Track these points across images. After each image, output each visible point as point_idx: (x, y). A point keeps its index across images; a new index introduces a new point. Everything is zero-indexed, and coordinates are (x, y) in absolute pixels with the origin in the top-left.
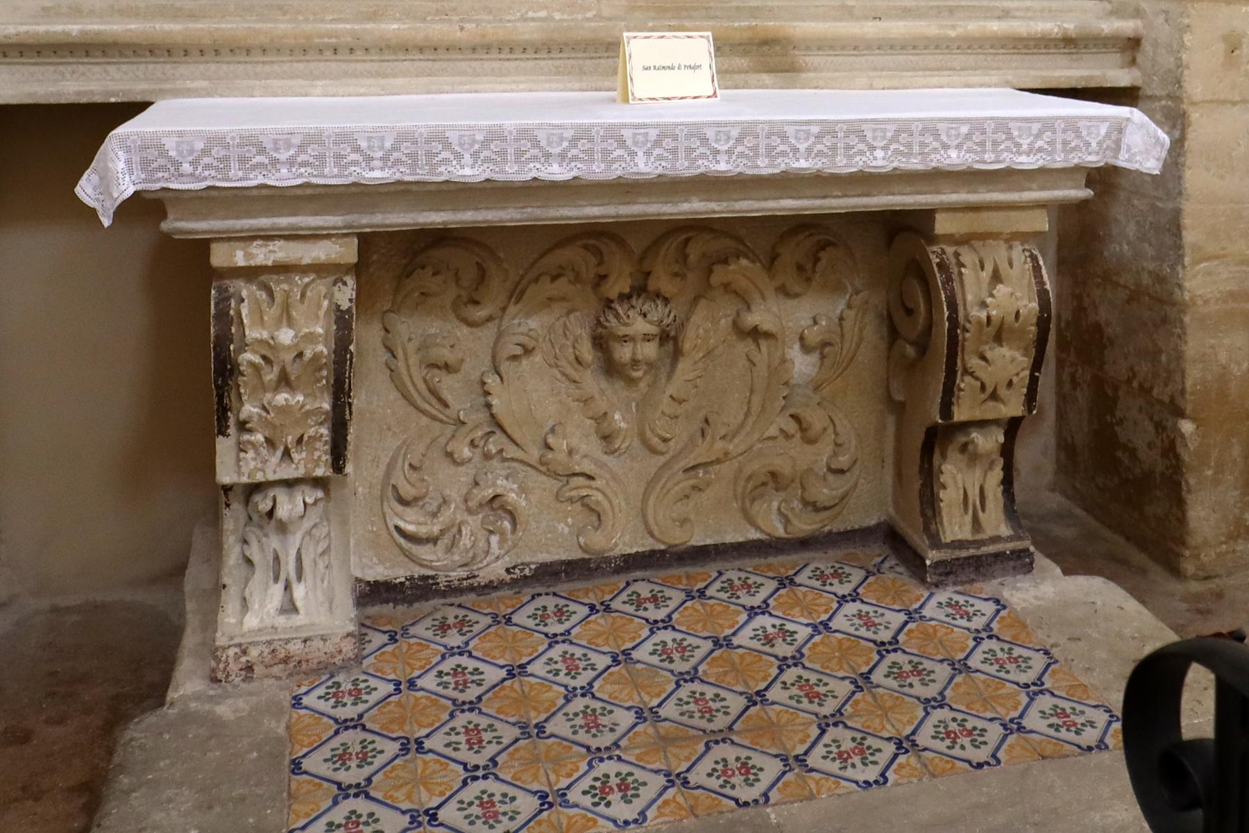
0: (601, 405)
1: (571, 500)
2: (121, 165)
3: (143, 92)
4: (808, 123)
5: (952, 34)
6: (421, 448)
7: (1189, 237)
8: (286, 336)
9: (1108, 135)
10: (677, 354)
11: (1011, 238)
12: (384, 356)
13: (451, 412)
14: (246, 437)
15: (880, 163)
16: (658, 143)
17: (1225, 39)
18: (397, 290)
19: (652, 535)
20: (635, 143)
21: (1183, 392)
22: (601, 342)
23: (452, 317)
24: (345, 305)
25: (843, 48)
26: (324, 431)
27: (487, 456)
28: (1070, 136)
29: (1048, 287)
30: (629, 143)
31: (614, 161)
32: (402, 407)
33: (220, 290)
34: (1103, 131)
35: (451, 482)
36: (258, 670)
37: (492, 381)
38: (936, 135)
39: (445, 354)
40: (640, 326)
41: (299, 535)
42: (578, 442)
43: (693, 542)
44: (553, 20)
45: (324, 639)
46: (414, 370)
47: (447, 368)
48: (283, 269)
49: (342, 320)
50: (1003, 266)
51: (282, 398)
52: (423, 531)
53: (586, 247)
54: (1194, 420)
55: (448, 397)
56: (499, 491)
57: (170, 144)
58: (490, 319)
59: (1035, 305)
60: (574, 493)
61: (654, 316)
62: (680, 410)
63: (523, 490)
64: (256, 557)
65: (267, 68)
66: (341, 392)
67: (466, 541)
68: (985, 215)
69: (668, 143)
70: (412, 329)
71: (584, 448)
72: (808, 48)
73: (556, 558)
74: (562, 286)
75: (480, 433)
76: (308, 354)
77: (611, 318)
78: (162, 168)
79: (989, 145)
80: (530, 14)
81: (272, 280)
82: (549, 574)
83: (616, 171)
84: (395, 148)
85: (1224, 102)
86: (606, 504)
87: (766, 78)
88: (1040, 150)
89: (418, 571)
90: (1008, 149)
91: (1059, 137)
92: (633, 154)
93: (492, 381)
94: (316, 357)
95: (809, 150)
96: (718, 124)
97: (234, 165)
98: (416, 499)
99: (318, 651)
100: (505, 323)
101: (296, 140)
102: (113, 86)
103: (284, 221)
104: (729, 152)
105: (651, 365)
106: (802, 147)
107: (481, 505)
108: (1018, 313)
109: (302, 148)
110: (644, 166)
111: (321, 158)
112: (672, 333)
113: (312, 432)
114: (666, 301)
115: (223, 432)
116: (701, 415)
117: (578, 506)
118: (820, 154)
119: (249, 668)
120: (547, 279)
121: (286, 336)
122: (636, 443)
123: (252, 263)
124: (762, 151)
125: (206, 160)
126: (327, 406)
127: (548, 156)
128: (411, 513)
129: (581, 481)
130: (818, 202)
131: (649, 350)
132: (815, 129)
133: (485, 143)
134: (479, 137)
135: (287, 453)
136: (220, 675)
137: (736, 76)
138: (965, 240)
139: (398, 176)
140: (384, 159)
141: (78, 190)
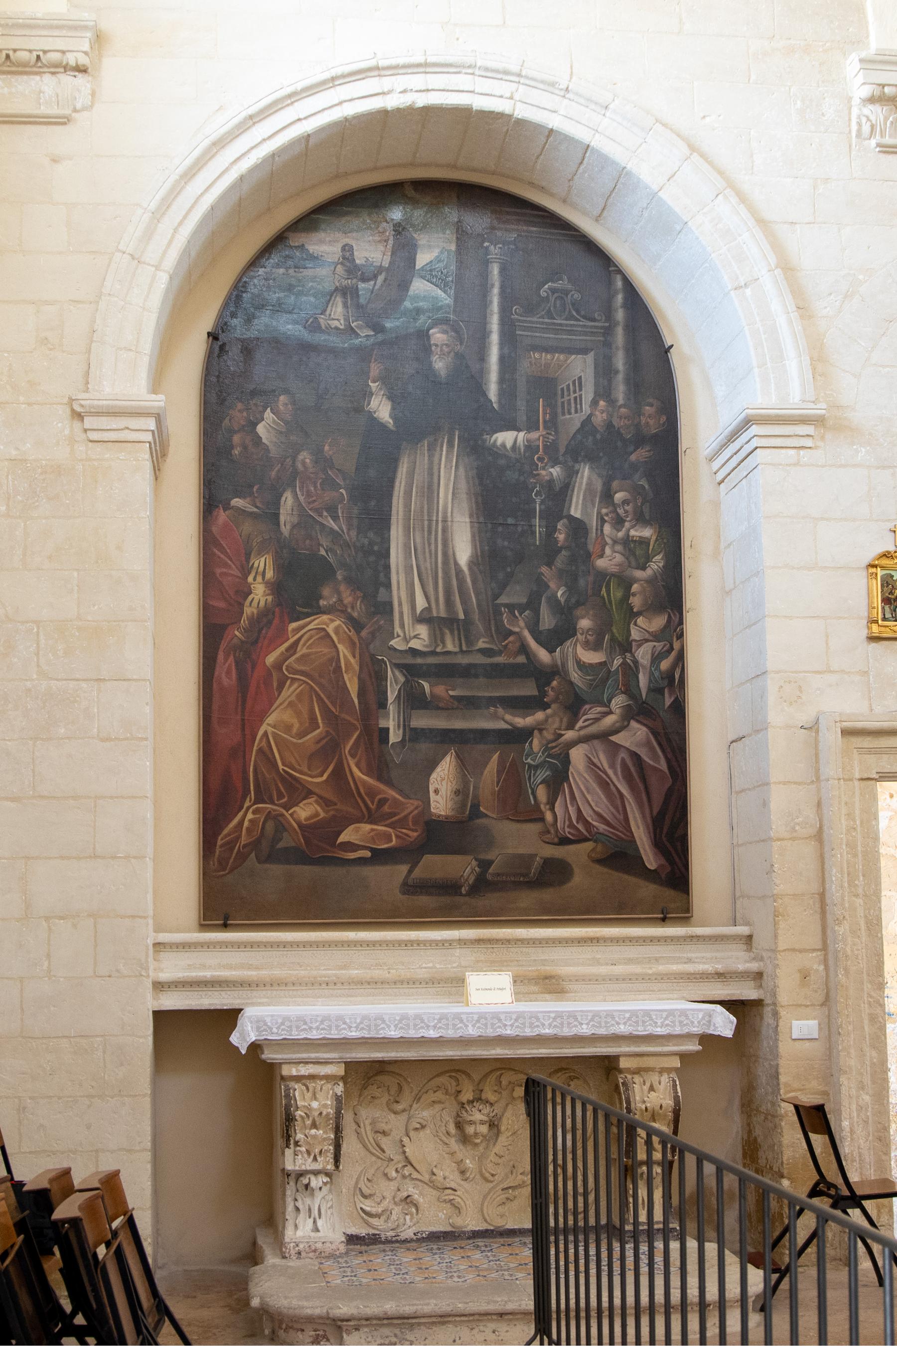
0: (459, 1156)
1: (445, 1201)
2: (250, 1028)
3: (239, 1004)
4: (550, 1012)
5: (650, 972)
6: (372, 1171)
7: (783, 1079)
8: (315, 1104)
9: (703, 1018)
10: (498, 1133)
11: (662, 1071)
12: (354, 1126)
13: (387, 1155)
14: (298, 1148)
15: (585, 1031)
16: (478, 1021)
17: (800, 971)
18: (360, 1095)
19: (486, 1221)
20: (468, 1021)
21: (782, 1163)
22: (459, 1126)
23: (386, 1109)
24: (339, 1094)
25: (590, 980)
26: (331, 1148)
27: (404, 1177)
28: (683, 1018)
29: (680, 1094)
30: (465, 1021)
31: (458, 1029)
32: (363, 1152)
33: (285, 1086)
34: (700, 1016)
35: (387, 1189)
36: (303, 1254)
37: (406, 1140)
38: (613, 1018)
39: (383, 1126)
40: (478, 1116)
41: (319, 1198)
42: (448, 1173)
43: (507, 1227)
44: (435, 968)
45: (331, 1243)
46: (369, 1133)
47: (384, 1133)
48: (312, 1077)
49: (338, 1099)
50: (656, 1085)
51: (313, 1131)
52: (373, 1211)
53: (450, 1077)
54: (789, 1179)
55: (384, 1146)
56: (410, 1193)
57: (268, 1020)
58: (404, 1110)
59: (671, 1103)
60: (446, 1197)
61: (485, 1111)
62: (500, 1161)
63: (421, 1194)
64: (301, 1207)
65: (295, 993)
66: (338, 1130)
67: (394, 1217)
68: (645, 1058)
69: (483, 1021)
70: (367, 1114)
71: (451, 1177)
72: (570, 980)
73: (439, 1230)
74: (439, 1095)
75: (400, 1166)
76: (324, 1113)
77: (463, 1112)
78: (265, 1030)
79: (640, 1023)
80: (424, 965)
81: (307, 1082)
82: (435, 1237)
83: (459, 1034)
84: (361, 1023)
85: (800, 1006)
86: (462, 1204)
87: (547, 996)
88: (667, 1025)
89: (372, 1231)
90: (650, 1025)
91: (677, 1019)
92: (467, 1026)
93: (406, 1140)
94: (328, 1114)
95: (550, 1025)
96: (506, 1013)
97: (294, 1029)
98: (371, 1195)
99: (328, 1248)
100: (411, 1113)
101: (319, 1019)
102: (225, 1001)
103: (313, 1055)
104: (512, 1025)
105: (484, 1136)
106: (547, 1023)
107: (401, 1201)
108: (661, 1107)
109: (322, 1022)
110: (472, 1031)
111: (330, 1027)
112: (496, 1123)
113: (326, 1148)
114: (492, 1104)
115: (288, 1146)
116: (511, 1163)
117: (449, 1205)
118: (555, 1026)
119: (299, 1253)
120: (431, 1092)
121: (315, 1104)
122: (478, 1177)
123: (299, 1074)
124: (527, 1025)
125: (283, 1027)
126: (332, 1136)
127: (428, 1026)
128: (367, 1202)
129: (450, 1191)
130: (558, 1051)
131: (484, 1129)
132: (553, 1015)
133: (400, 1021)
134: (398, 1018)
135: (315, 1159)
136: (287, 1255)
137: (531, 996)
138: (638, 1071)
139: (363, 1035)
140: (357, 1027)
141: (231, 1039)
